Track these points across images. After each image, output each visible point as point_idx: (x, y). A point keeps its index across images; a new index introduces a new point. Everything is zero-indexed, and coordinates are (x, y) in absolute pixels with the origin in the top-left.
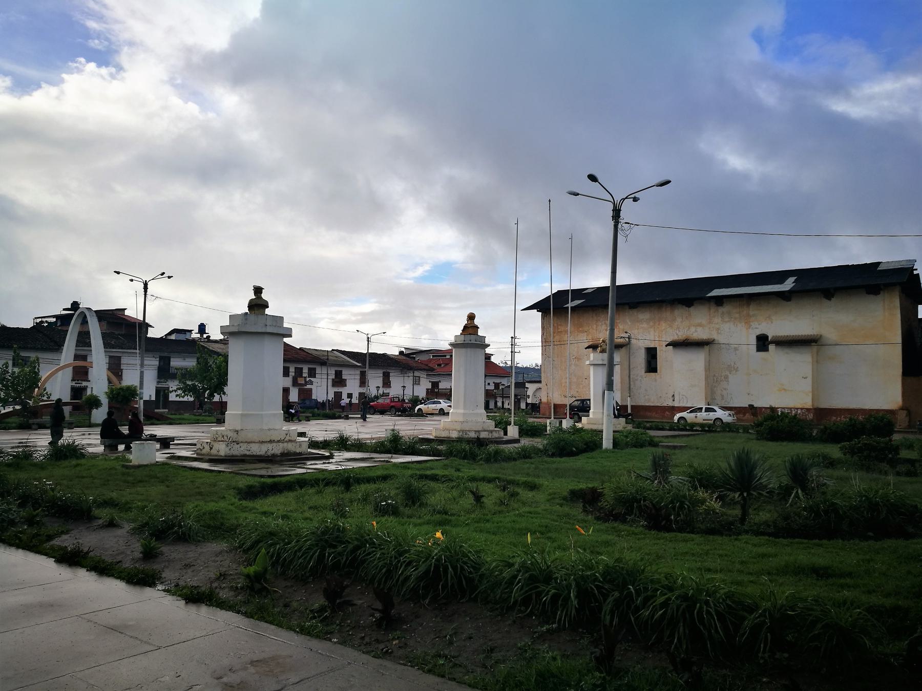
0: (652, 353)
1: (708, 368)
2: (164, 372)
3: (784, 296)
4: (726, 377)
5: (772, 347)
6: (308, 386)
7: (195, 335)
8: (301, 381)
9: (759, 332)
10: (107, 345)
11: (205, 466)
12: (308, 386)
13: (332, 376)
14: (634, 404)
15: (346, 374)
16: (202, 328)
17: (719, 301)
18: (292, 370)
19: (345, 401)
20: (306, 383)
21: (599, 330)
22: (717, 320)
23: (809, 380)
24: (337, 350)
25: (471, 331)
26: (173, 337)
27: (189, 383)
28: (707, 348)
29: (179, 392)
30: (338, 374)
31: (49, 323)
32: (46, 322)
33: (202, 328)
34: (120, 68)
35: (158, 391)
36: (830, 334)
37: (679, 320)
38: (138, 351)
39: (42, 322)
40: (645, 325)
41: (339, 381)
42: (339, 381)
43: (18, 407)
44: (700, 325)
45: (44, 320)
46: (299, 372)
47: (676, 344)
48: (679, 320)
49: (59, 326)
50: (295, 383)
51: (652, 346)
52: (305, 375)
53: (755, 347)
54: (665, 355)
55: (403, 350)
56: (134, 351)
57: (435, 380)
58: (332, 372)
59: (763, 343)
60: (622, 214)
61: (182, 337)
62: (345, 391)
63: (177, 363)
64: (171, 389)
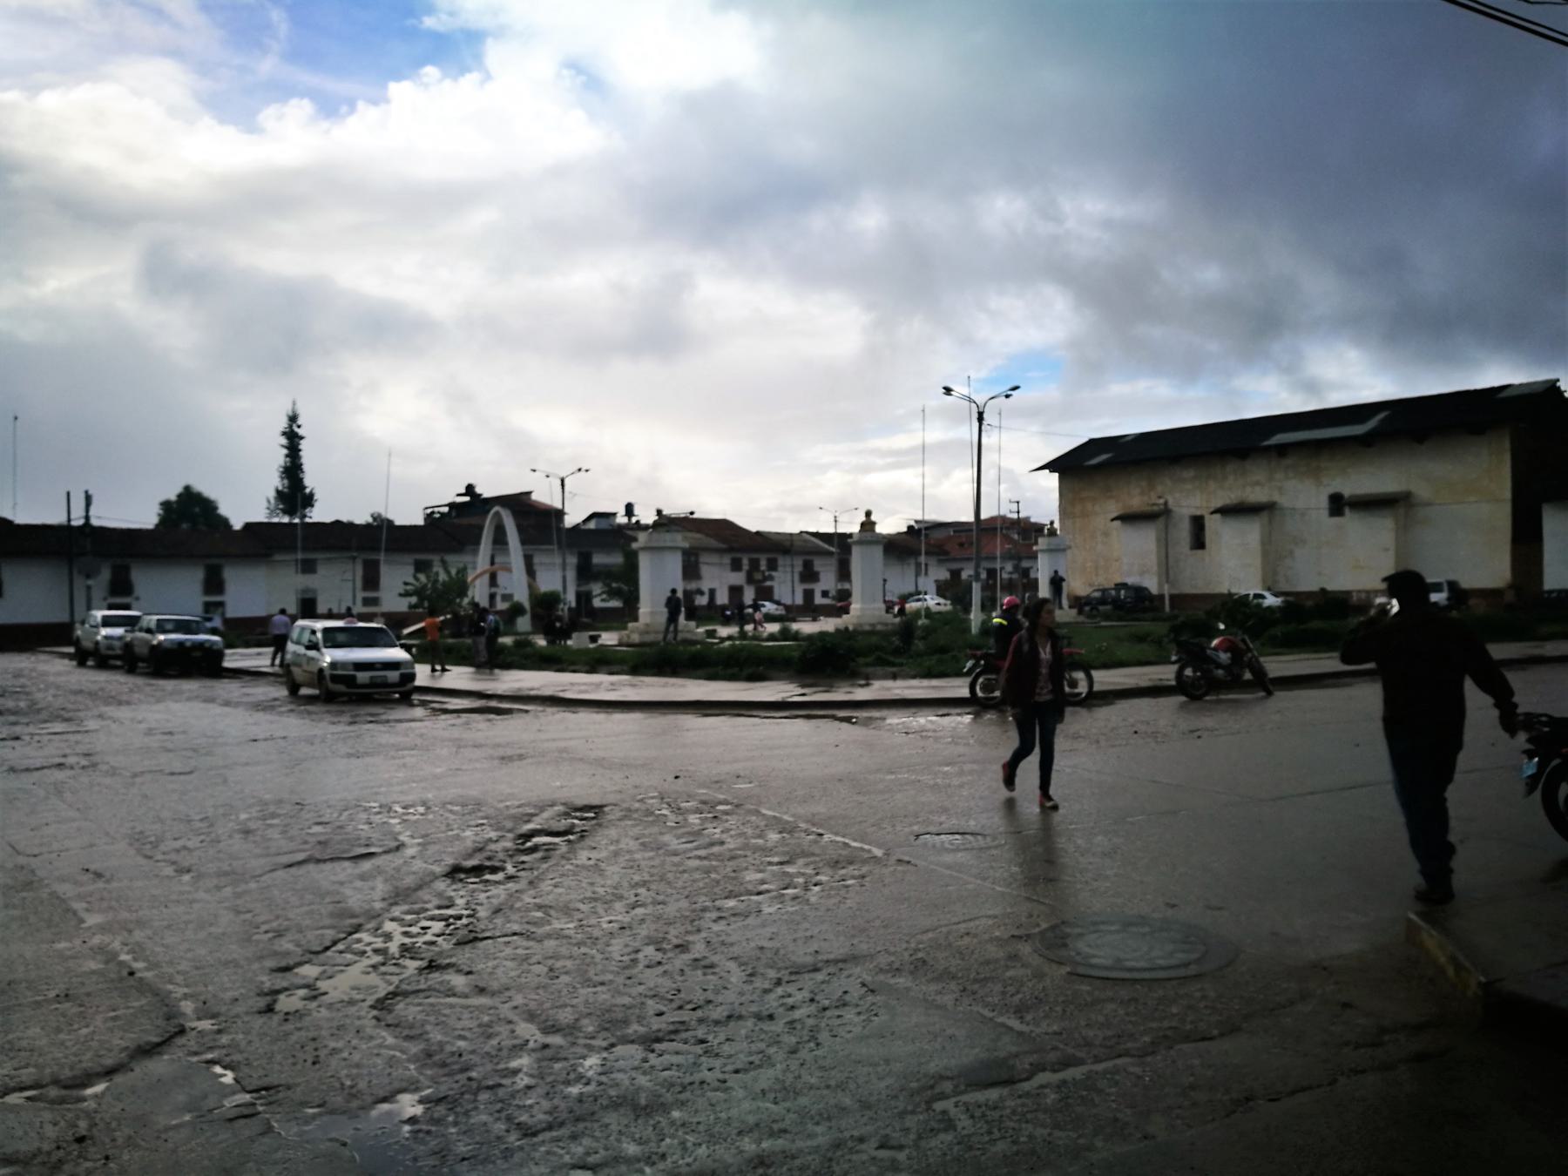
0: (1198, 523)
1: (1267, 543)
2: (586, 572)
3: (1366, 442)
4: (1291, 553)
5: (1347, 510)
6: (768, 583)
7: (622, 519)
8: (758, 576)
9: (1332, 490)
10: (523, 542)
11: (625, 649)
12: (768, 583)
13: (799, 568)
14: (1175, 592)
15: (818, 564)
16: (629, 509)
17: (1283, 450)
18: (745, 562)
19: (819, 600)
20: (766, 579)
21: (1136, 497)
22: (1279, 475)
23: (1392, 553)
24: (807, 533)
25: (867, 527)
26: (592, 525)
27: (614, 585)
28: (1265, 515)
29: (604, 596)
30: (808, 565)
31: (442, 514)
32: (439, 512)
33: (629, 509)
34: (488, 77)
35: (579, 596)
36: (1421, 490)
37: (1231, 478)
38: (556, 547)
39: (433, 513)
40: (1189, 486)
41: (809, 575)
42: (809, 575)
43: (449, 616)
44: (1258, 483)
45: (436, 510)
46: (754, 565)
47: (1226, 511)
48: (1231, 478)
49: (455, 517)
50: (750, 580)
51: (1198, 513)
52: (763, 568)
53: (1326, 512)
54: (1213, 524)
55: (913, 523)
56: (551, 547)
57: (955, 566)
58: (798, 564)
59: (1338, 505)
60: (985, 416)
61: (604, 524)
62: (818, 588)
63: (598, 559)
64: (594, 593)
